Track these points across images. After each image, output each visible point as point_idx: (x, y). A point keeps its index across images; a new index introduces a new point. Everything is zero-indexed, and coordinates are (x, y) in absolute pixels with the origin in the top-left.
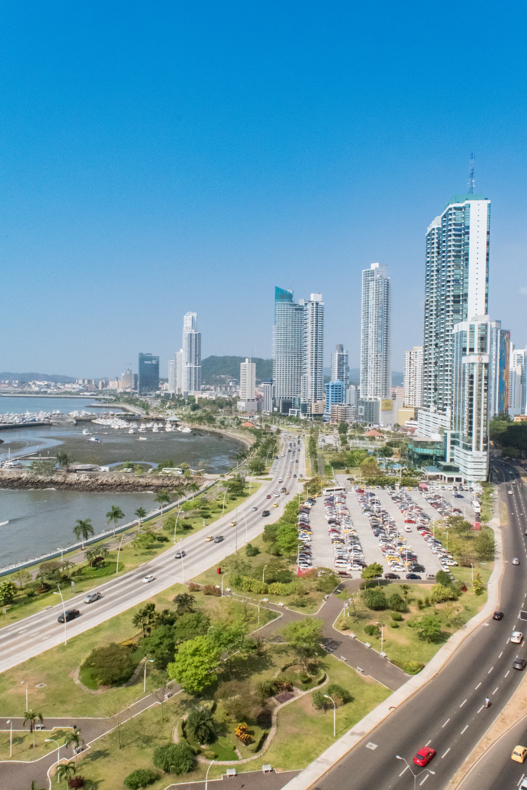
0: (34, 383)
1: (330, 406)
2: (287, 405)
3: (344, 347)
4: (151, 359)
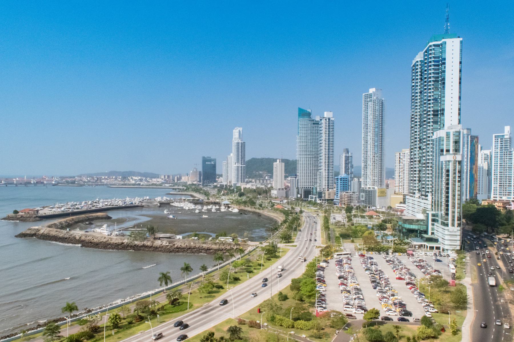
0: (132, 178)
1: (339, 193)
2: (307, 193)
4: (210, 160)
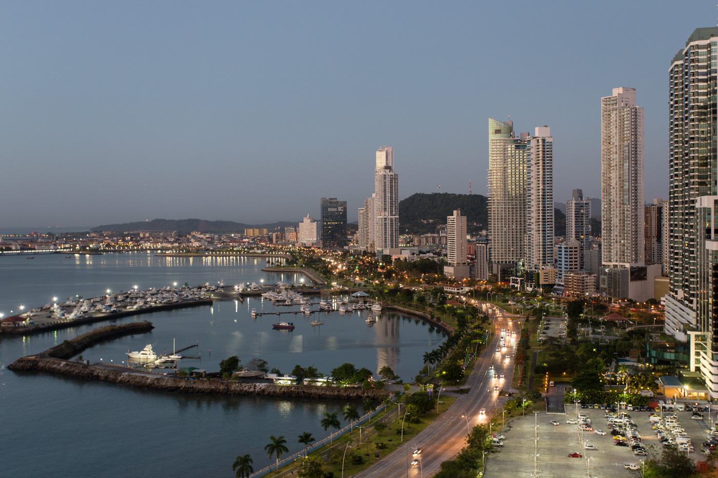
0: (194, 237)
2: (507, 271)
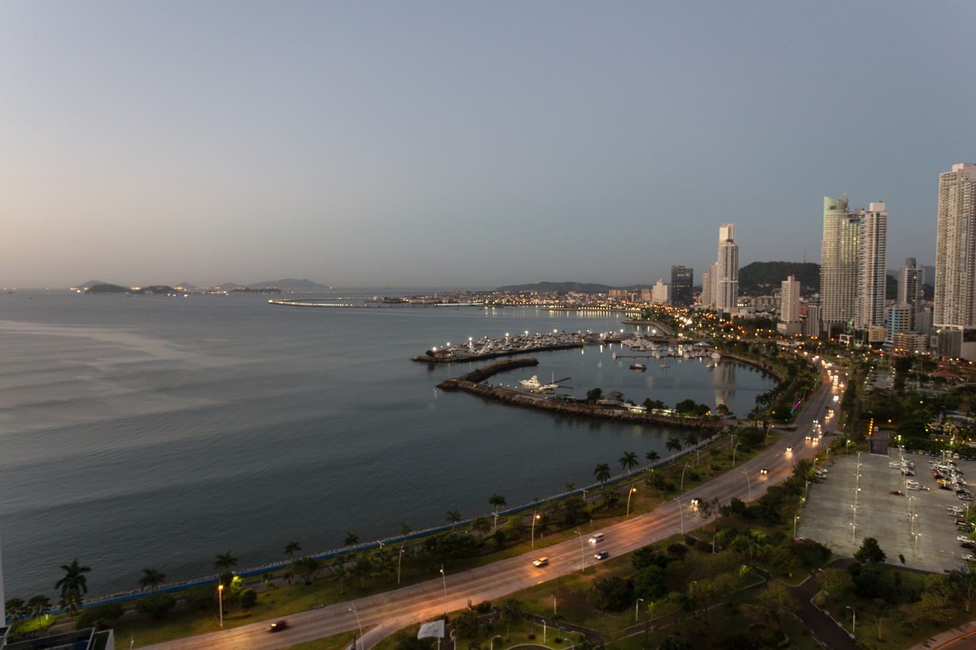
0: (570, 295)
1: (893, 333)
2: (838, 329)
3: (917, 261)
4: (685, 271)
